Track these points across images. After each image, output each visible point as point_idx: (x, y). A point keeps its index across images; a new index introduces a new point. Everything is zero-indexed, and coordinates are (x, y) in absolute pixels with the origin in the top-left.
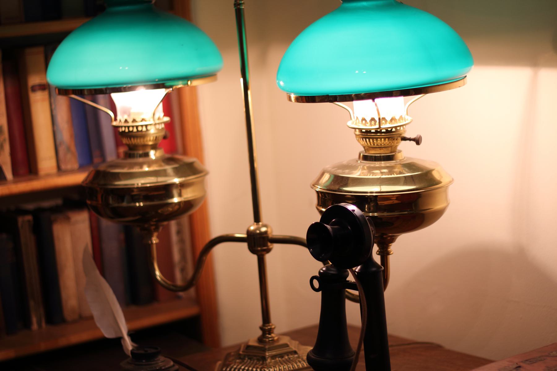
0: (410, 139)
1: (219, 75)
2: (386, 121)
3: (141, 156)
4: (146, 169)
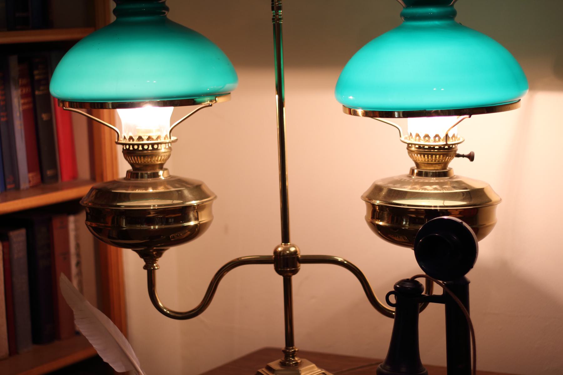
0: (463, 156)
1: (232, 93)
2: (440, 138)
3: (150, 176)
4: (150, 190)
